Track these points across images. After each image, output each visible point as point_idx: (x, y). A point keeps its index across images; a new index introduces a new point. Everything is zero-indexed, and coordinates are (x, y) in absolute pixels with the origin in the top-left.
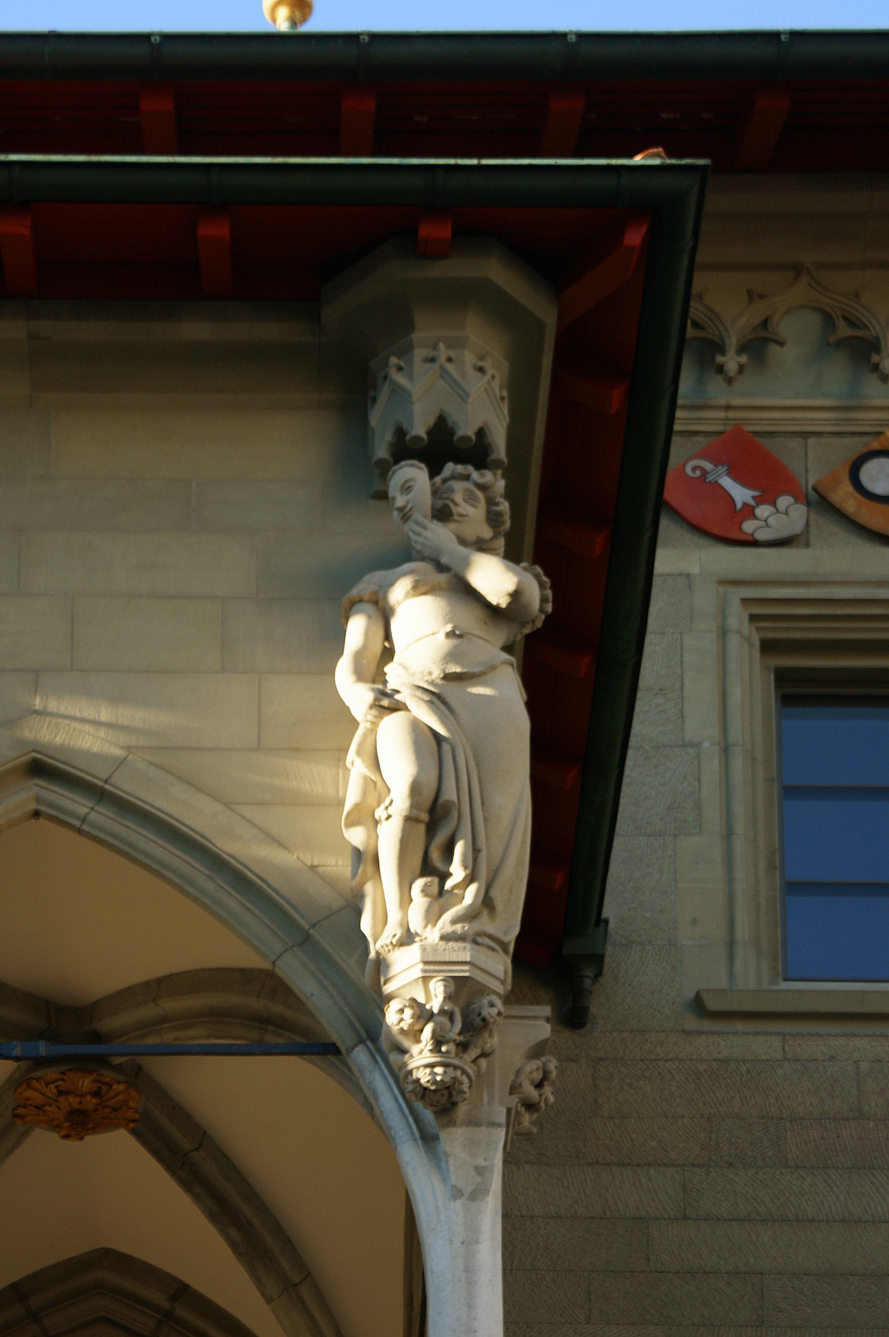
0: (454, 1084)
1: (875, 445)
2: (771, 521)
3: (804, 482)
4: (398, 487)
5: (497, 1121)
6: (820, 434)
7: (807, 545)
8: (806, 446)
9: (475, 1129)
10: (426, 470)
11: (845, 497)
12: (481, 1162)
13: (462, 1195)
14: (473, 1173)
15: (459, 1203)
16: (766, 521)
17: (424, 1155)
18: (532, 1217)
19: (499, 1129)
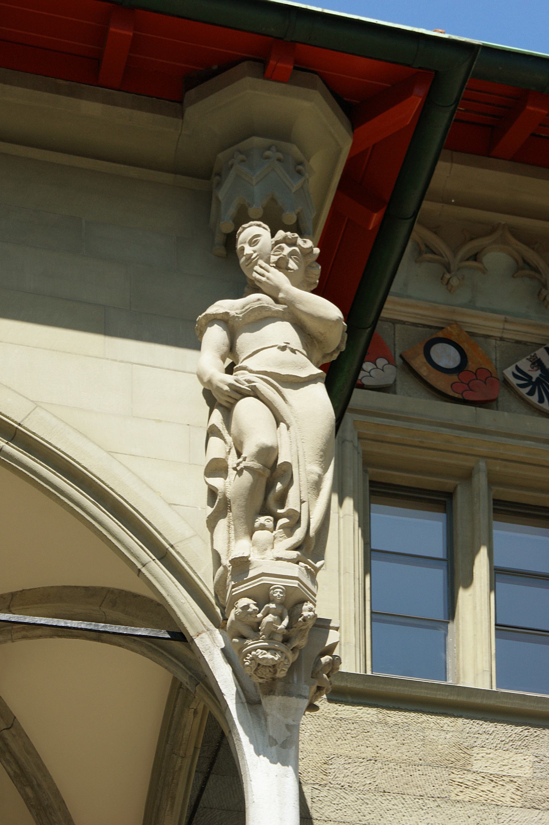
0: (280, 664)
1: (440, 334)
2: (372, 373)
3: (393, 352)
4: (248, 241)
5: (303, 694)
6: (403, 323)
7: (395, 393)
8: (395, 328)
9: (288, 698)
10: (269, 230)
11: (419, 363)
12: (291, 722)
13: (277, 743)
14: (284, 728)
15: (274, 749)
16: (369, 372)
17: (249, 714)
18: (211, 808)
19: (305, 700)
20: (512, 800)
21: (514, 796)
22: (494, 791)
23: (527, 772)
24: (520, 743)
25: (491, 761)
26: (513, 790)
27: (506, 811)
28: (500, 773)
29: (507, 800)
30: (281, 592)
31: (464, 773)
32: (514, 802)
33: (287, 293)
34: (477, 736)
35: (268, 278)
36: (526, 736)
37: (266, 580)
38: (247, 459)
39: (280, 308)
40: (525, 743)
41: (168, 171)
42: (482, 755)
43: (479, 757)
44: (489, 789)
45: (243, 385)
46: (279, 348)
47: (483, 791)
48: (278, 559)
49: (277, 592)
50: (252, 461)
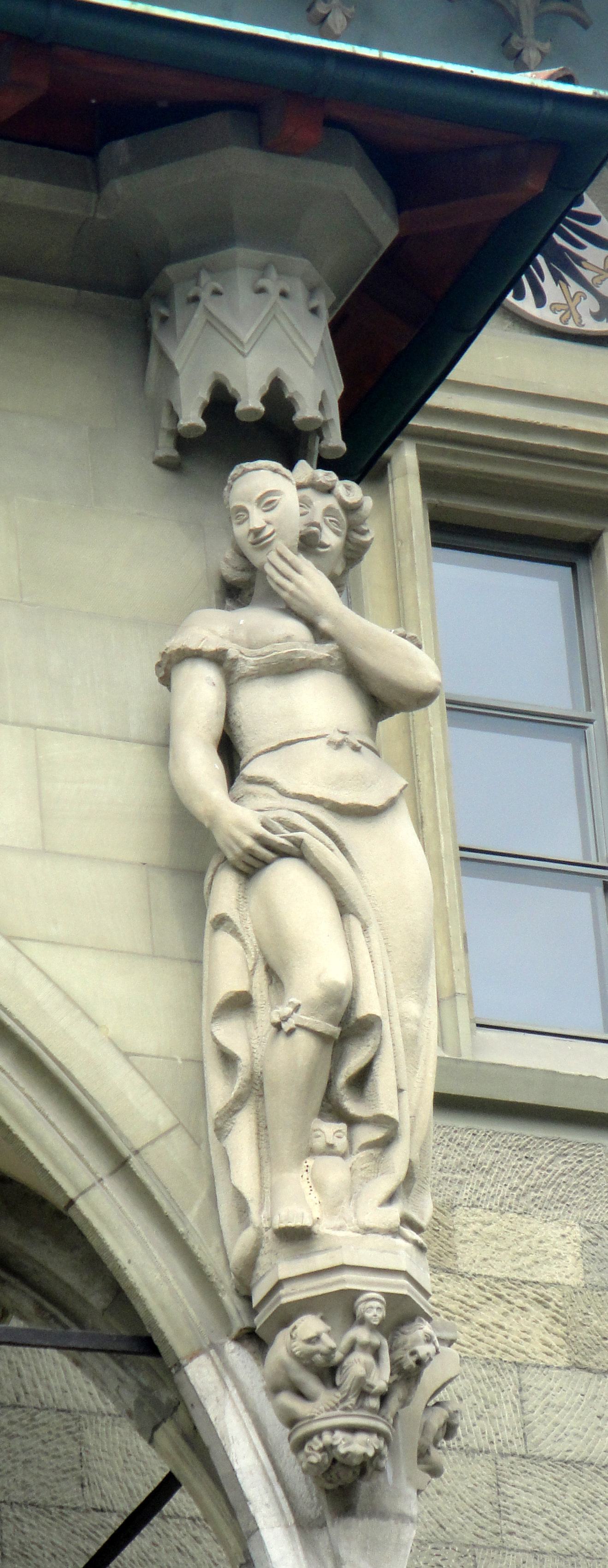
20: (547, 1349)
21: (549, 1338)
22: (506, 1325)
23: (567, 1270)
24: (550, 1192)
25: (495, 1243)
26: (546, 1322)
27: (536, 1380)
28: (514, 1275)
29: (537, 1349)
30: (378, 1308)
31: (441, 1280)
32: (551, 1355)
33: (335, 620)
34: (459, 1176)
35: (299, 586)
36: (563, 1174)
37: (351, 1281)
38: (301, 1010)
39: (322, 651)
40: (561, 1192)
41: (56, 281)
42: (474, 1227)
43: (467, 1233)
44: (496, 1320)
45: (274, 833)
46: (330, 743)
47: (483, 1326)
48: (367, 1230)
49: (372, 1307)
50: (312, 1015)
